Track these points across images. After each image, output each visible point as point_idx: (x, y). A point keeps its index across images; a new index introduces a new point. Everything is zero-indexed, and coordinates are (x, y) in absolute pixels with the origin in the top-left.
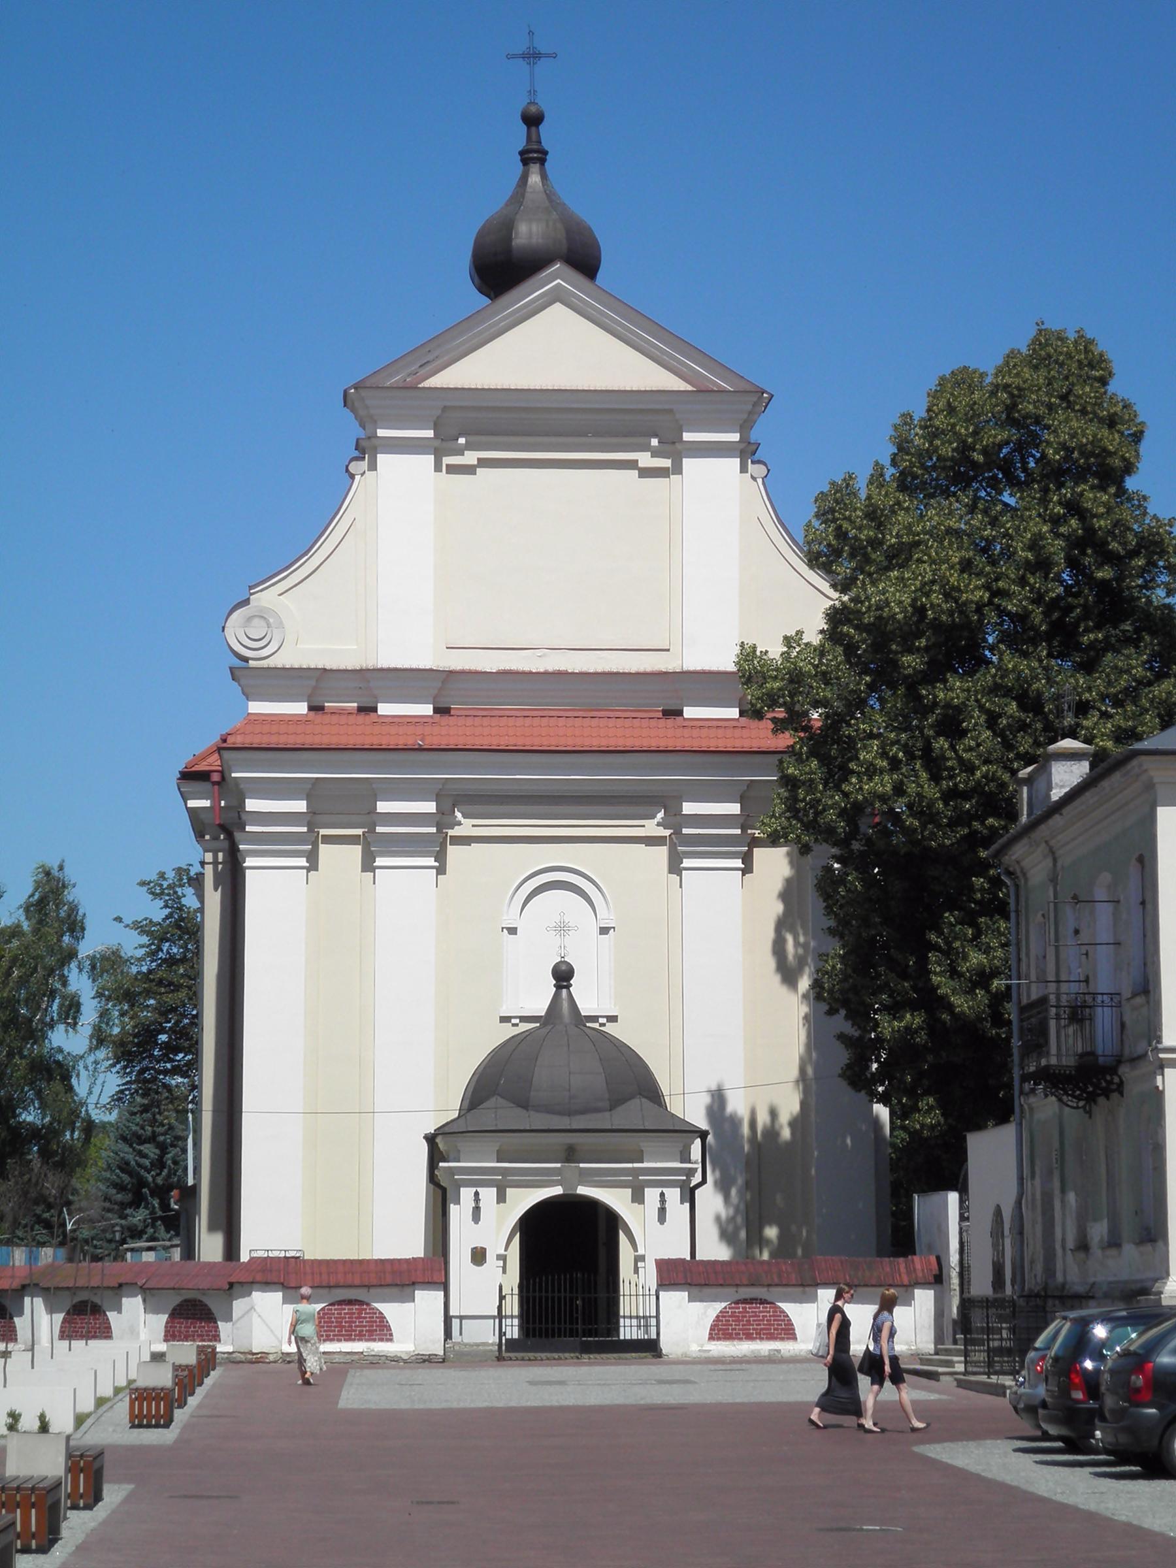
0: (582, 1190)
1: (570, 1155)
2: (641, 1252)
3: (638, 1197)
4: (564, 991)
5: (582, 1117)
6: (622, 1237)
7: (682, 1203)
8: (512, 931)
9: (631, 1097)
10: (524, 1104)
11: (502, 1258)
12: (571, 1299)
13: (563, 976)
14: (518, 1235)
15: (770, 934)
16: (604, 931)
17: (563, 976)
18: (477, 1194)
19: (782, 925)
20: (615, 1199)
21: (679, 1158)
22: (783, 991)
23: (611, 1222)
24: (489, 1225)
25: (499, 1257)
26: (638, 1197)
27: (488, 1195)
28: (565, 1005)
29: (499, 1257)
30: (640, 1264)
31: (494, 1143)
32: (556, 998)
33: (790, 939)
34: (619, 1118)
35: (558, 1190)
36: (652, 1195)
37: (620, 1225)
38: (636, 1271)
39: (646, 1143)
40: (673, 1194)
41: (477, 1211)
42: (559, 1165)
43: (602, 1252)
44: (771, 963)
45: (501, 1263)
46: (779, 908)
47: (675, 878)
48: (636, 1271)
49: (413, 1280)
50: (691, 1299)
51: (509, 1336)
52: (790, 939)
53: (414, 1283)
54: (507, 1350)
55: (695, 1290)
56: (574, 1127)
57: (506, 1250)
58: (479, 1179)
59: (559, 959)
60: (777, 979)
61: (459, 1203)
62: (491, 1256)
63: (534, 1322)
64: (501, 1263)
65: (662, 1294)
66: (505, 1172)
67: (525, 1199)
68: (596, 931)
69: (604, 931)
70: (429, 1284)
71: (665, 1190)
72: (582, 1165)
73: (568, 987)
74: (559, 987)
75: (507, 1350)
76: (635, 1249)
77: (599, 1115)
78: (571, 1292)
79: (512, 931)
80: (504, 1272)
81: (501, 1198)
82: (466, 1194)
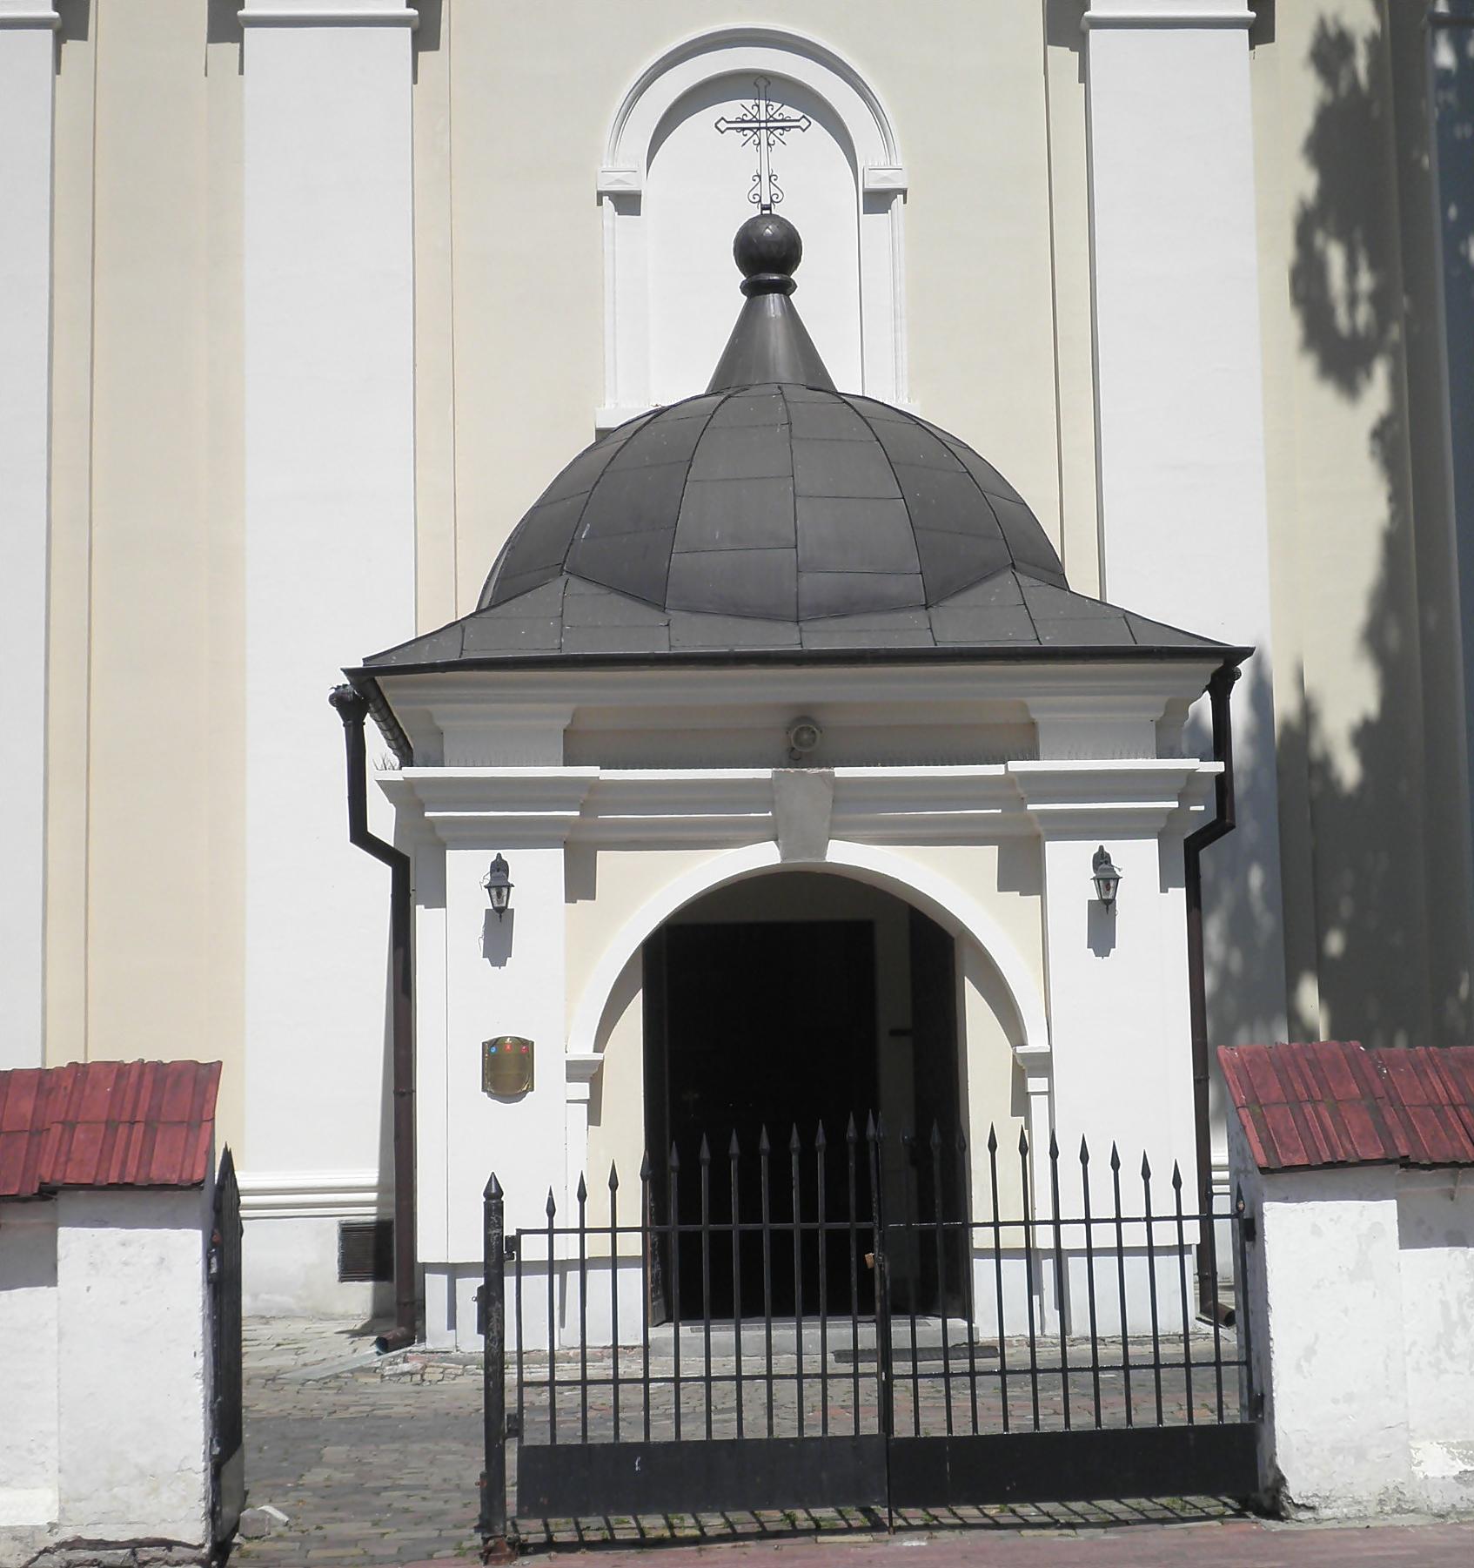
0: (843, 853)
1: (803, 741)
2: (1036, 1042)
3: (1022, 873)
4: (773, 301)
5: (833, 624)
6: (975, 1007)
7: (1164, 889)
8: (628, 203)
9: (987, 573)
10: (651, 592)
11: (589, 1073)
12: (837, 1241)
13: (768, 258)
14: (639, 997)
15: (1285, 252)
16: (877, 201)
17: (768, 258)
18: (500, 868)
19: (1307, 225)
20: (949, 879)
21: (1151, 742)
22: (1326, 396)
23: (933, 952)
24: (560, 960)
25: (576, 1071)
26: (1022, 873)
27: (538, 872)
28: (778, 342)
29: (576, 1071)
30: (1035, 1084)
31: (555, 702)
32: (748, 323)
33: (1336, 257)
34: (956, 625)
35: (764, 855)
36: (1068, 862)
37: (964, 958)
38: (1021, 1103)
39: (1043, 695)
40: (1139, 860)
41: (499, 922)
42: (766, 773)
43: (895, 1066)
44: (1291, 327)
45: (583, 1090)
46: (1305, 182)
47: (1065, 57)
48: (1021, 1103)
49: (46, 1173)
50: (1414, 1234)
51: (536, 1435)
52: (1336, 257)
53: (47, 1193)
54: (529, 1506)
55: (1428, 1187)
56: (815, 644)
57: (599, 1046)
58: (505, 822)
59: (756, 211)
60: (1305, 367)
61: (442, 903)
62: (548, 1068)
63: (720, 1212)
64: (583, 1090)
65: (1283, 1221)
66: (590, 796)
67: (658, 885)
68: (850, 200)
69: (877, 201)
70: (131, 1193)
71: (1111, 847)
72: (840, 772)
73: (786, 288)
74: (754, 289)
75: (529, 1506)
76: (1016, 1032)
77: (902, 618)
78: (837, 1211)
79: (628, 203)
80: (594, 1117)
81: (580, 884)
82: (466, 870)
